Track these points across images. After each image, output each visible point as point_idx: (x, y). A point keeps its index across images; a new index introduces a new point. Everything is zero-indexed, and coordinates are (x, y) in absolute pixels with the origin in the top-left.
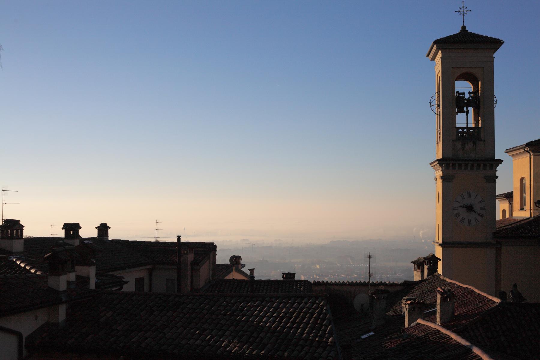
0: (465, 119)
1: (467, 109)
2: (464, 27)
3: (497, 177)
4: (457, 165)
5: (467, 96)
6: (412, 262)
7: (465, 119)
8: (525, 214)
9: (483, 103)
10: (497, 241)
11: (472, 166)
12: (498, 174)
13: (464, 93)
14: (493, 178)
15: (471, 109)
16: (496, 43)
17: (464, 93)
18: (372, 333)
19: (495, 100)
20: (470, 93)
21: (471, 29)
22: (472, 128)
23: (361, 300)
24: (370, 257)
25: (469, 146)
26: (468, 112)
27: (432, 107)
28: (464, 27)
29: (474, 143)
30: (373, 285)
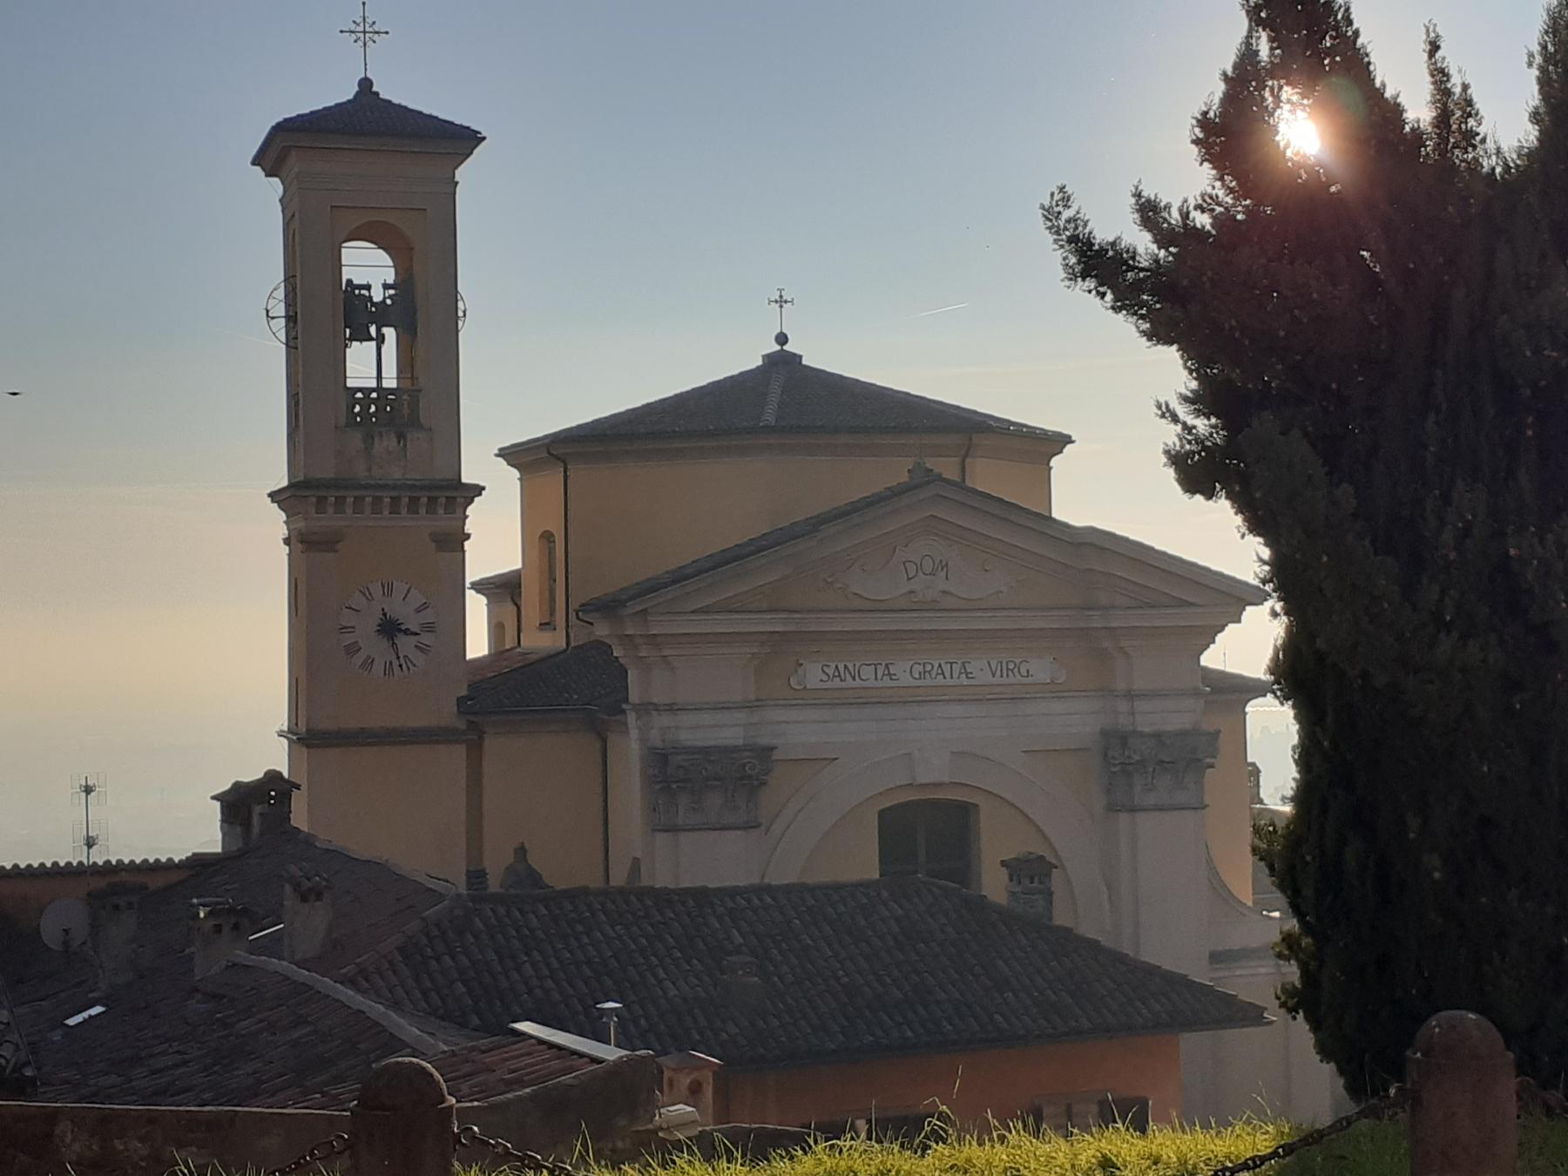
0: (368, 364)
1: (378, 330)
2: (366, 84)
3: (468, 536)
4: (350, 500)
5: (377, 295)
6: (213, 798)
7: (368, 364)
8: (552, 641)
9: (424, 311)
10: (470, 723)
11: (395, 507)
12: (469, 527)
13: (368, 287)
14: (456, 540)
15: (390, 332)
16: (464, 140)
17: (368, 287)
18: (98, 1009)
19: (460, 304)
20: (386, 287)
21: (386, 90)
22: (391, 391)
23: (60, 921)
24: (88, 790)
25: (387, 443)
26: (380, 339)
27: (272, 322)
28: (366, 84)
29: (401, 436)
30: (95, 870)
